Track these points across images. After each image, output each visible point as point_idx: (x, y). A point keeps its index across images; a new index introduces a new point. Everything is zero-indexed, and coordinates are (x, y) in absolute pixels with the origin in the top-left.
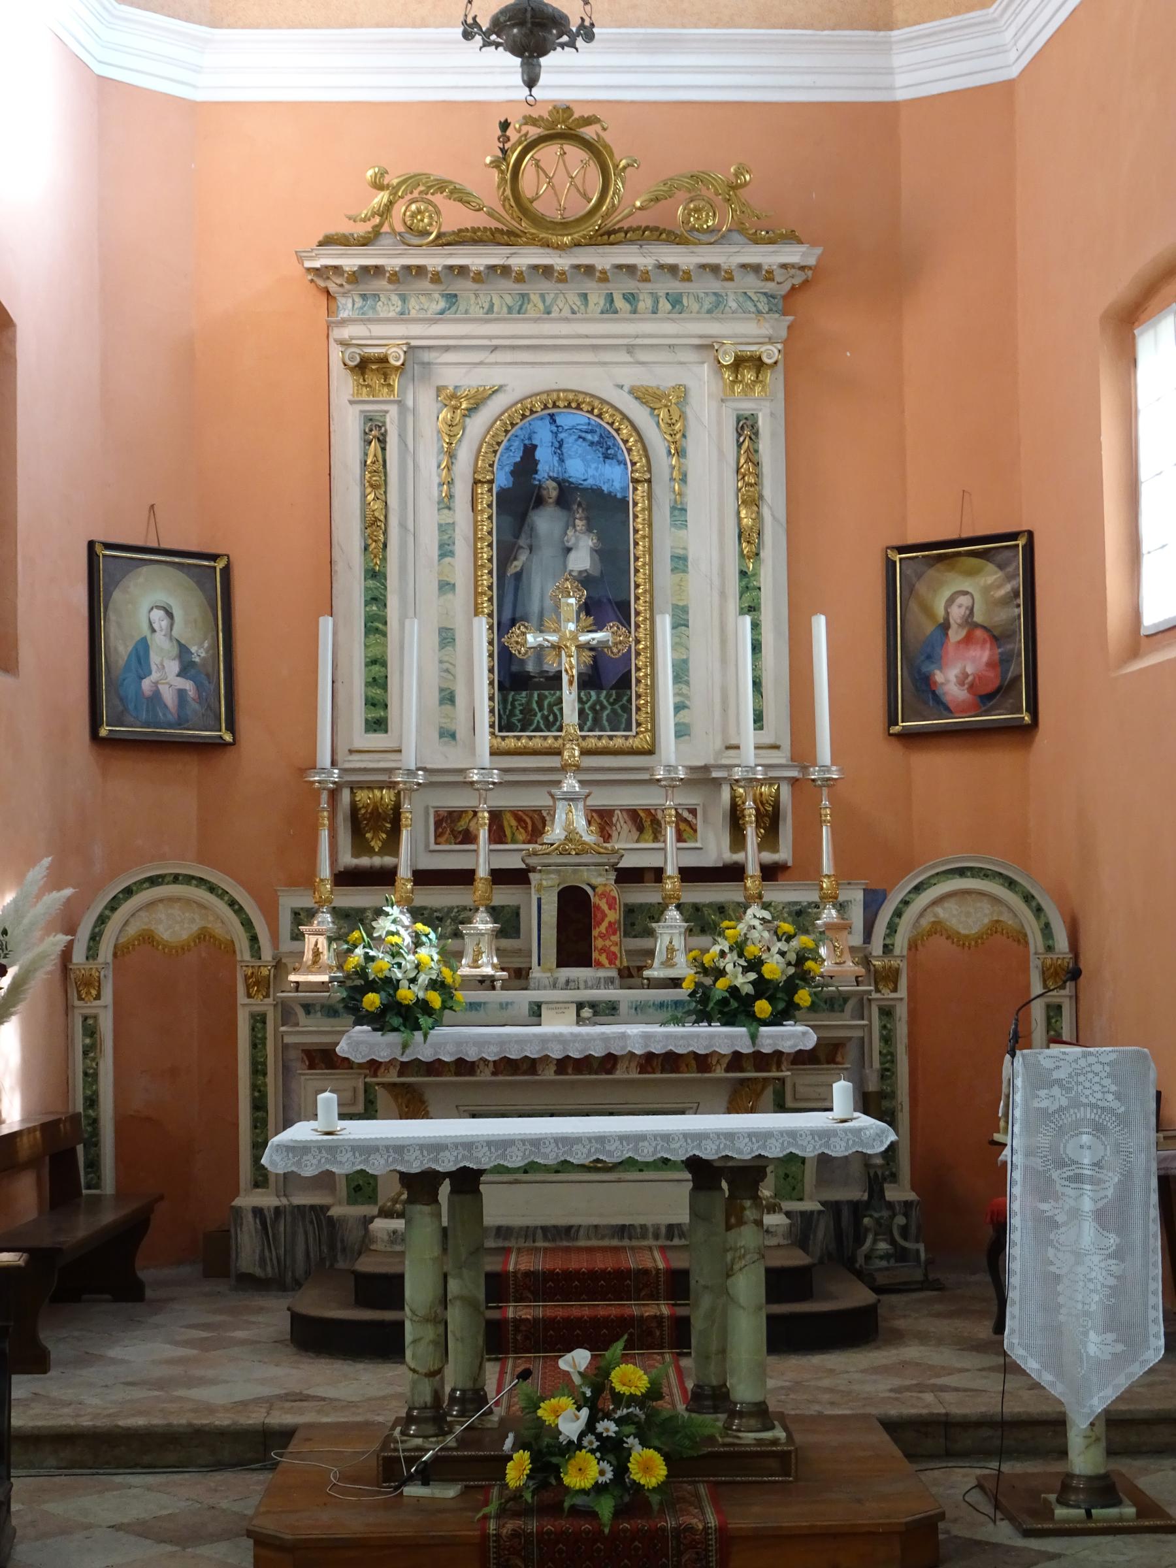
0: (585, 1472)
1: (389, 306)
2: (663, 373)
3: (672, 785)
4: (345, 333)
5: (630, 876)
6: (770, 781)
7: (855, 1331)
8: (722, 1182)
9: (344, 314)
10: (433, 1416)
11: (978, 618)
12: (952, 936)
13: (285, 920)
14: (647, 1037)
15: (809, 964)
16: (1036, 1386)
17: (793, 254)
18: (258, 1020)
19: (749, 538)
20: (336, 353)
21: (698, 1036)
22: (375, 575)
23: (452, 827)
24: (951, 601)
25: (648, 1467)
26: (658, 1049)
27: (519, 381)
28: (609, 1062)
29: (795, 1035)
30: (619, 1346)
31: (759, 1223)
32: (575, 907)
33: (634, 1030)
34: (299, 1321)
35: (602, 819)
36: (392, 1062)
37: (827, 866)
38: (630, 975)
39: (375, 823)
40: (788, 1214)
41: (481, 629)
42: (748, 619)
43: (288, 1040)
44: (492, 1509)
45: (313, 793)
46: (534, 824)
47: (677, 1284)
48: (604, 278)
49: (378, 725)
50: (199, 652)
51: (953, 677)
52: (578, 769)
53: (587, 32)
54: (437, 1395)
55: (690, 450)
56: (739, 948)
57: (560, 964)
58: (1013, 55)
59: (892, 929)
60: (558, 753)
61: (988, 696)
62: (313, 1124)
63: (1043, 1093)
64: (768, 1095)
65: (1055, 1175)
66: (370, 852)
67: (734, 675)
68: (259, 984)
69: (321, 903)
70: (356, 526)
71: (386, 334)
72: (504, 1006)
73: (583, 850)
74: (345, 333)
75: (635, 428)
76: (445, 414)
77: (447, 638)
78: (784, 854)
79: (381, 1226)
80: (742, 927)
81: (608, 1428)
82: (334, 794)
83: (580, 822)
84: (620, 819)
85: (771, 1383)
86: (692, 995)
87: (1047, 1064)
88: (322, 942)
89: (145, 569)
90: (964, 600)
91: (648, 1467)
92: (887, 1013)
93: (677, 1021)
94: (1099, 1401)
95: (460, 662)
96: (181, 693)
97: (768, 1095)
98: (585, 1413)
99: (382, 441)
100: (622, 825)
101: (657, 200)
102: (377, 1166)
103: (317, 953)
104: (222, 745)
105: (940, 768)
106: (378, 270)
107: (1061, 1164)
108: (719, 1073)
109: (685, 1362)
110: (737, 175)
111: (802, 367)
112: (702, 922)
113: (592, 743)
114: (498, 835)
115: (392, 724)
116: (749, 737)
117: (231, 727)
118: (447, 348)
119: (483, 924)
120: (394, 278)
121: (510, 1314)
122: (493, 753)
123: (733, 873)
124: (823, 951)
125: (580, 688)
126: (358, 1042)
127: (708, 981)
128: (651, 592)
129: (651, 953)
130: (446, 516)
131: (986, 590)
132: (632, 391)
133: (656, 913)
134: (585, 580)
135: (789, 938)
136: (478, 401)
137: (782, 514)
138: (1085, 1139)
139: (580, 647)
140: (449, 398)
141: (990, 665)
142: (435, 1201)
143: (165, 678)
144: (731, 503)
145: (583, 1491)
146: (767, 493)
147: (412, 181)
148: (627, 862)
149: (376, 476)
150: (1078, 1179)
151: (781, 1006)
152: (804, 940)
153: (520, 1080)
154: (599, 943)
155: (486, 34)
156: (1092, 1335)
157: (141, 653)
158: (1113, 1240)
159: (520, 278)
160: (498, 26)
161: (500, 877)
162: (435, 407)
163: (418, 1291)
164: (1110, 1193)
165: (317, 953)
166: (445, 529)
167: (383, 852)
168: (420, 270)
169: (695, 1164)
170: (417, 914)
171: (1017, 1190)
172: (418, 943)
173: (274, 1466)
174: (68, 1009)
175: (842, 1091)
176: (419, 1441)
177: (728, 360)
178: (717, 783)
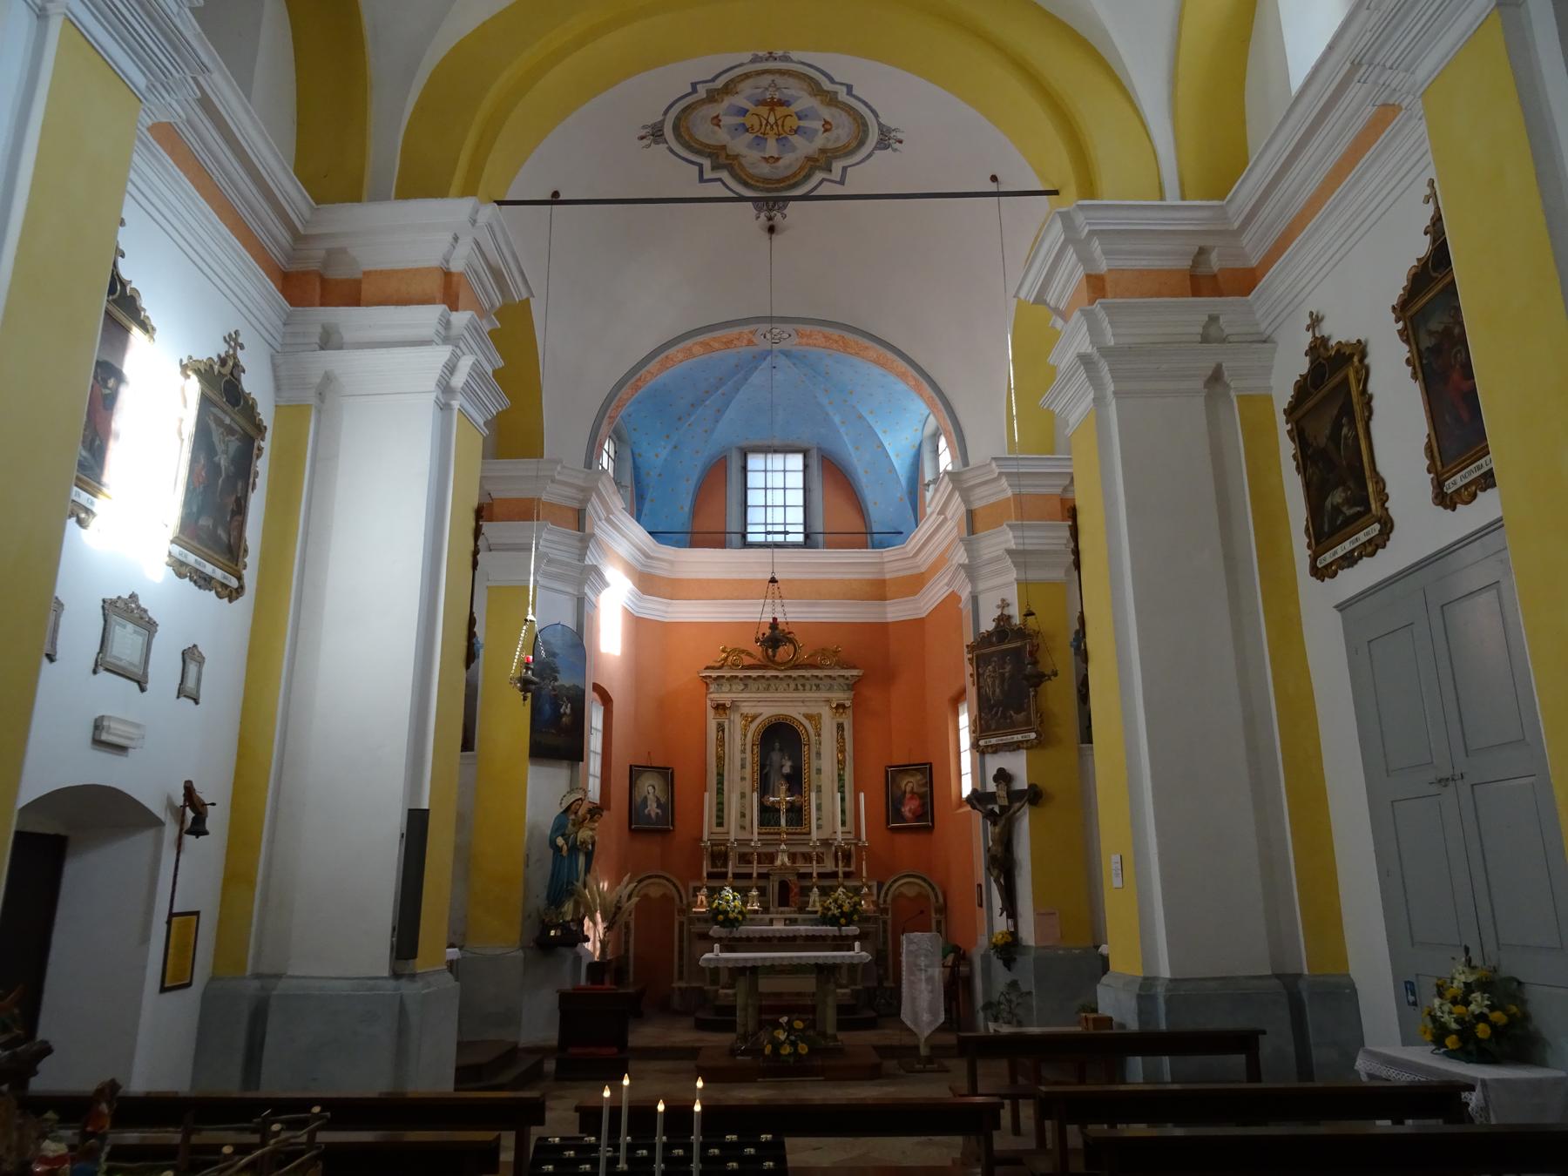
0: (786, 1050)
1: (726, 687)
2: (813, 706)
3: (814, 847)
17: (855, 672)
18: (681, 924)
19: (841, 763)
22: (720, 775)
23: (744, 859)
25: (803, 1049)
28: (794, 938)
29: (853, 930)
32: (784, 887)
35: (793, 857)
38: (802, 910)
39: (719, 857)
41: (755, 795)
46: (771, 858)
49: (720, 824)
50: (663, 800)
51: (906, 810)
56: (836, 901)
67: (835, 809)
68: (682, 911)
71: (725, 697)
77: (743, 795)
78: (852, 869)
91: (803, 1049)
92: (885, 923)
100: (799, 858)
104: (668, 831)
105: (904, 840)
112: (825, 892)
114: (759, 862)
116: (839, 829)
119: (754, 893)
123: (834, 875)
126: (715, 930)
133: (810, 889)
136: (754, 718)
143: (652, 809)
147: (734, 650)
149: (721, 742)
153: (766, 942)
161: (760, 876)
166: (743, 760)
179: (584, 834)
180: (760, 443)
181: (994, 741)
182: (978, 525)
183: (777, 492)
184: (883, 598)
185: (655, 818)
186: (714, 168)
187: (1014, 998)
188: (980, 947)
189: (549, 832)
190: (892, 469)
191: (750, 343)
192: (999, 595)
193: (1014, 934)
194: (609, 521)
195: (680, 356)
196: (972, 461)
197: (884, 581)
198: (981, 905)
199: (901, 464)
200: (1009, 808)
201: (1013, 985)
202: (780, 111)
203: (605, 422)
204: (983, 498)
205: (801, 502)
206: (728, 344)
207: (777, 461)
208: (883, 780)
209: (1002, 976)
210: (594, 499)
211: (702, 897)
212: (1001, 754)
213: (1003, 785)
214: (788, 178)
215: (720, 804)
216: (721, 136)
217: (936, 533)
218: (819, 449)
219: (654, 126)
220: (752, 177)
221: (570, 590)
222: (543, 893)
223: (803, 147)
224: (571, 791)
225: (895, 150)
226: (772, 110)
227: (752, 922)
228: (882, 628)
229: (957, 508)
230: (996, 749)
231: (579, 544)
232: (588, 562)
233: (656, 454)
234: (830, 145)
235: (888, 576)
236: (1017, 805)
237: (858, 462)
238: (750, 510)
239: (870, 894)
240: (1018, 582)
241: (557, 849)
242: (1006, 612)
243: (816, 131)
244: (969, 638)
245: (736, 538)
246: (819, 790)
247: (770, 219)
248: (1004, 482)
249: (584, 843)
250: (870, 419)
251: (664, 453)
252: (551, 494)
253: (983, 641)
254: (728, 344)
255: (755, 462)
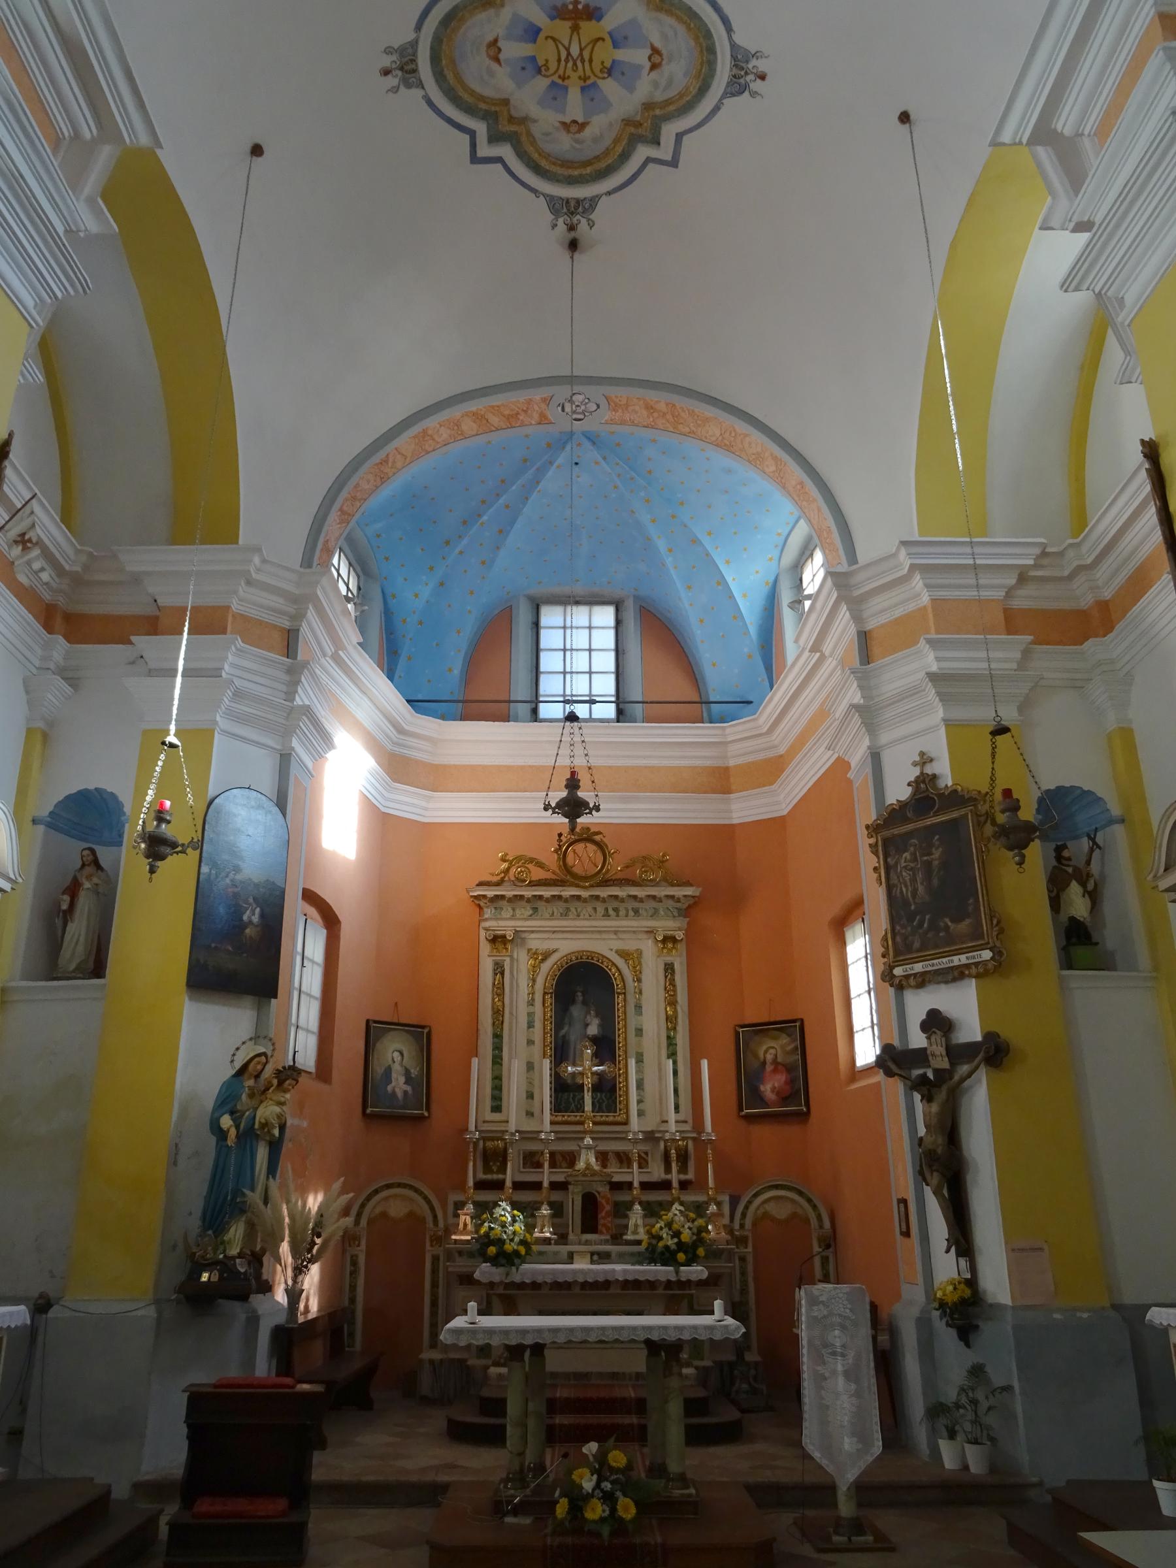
0: (595, 1511)
1: (507, 912)
3: (635, 1141)
4: (487, 924)
5: (616, 1186)
6: (683, 1139)
7: (729, 1434)
8: (662, 1351)
9: (486, 916)
10: (519, 1477)
11: (779, 1060)
12: (773, 1219)
13: (451, 1208)
14: (625, 1271)
15: (704, 1234)
16: (821, 1467)
17: (689, 891)
18: (436, 1259)
19: (671, 1020)
20: (483, 933)
21: (650, 1271)
22: (498, 1036)
23: (532, 1160)
24: (766, 1052)
26: (630, 1278)
27: (566, 947)
28: (607, 1284)
29: (697, 1271)
30: (612, 1439)
31: (680, 1374)
32: (590, 1203)
33: (618, 1267)
34: (451, 1423)
35: (603, 1157)
36: (501, 1282)
37: (711, 1183)
38: (617, 1238)
39: (495, 1157)
40: (696, 1368)
41: (547, 1063)
42: (671, 1061)
43: (450, 1269)
44: (549, 1530)
45: (466, 1143)
46: (571, 1159)
47: (640, 1406)
48: (604, 900)
49: (497, 1109)
50: (414, 1072)
51: (769, 1087)
52: (592, 1132)
53: (597, 808)
54: (522, 1465)
55: (643, 978)
56: (669, 1225)
57: (583, 1232)
58: (784, 806)
59: (744, 1215)
60: (582, 1123)
61: (786, 1098)
62: (464, 1318)
63: (815, 1308)
64: (685, 1304)
65: (823, 1351)
66: (492, 1172)
67: (663, 1087)
69: (468, 1199)
70: (490, 1013)
71: (505, 925)
72: (556, 1253)
73: (594, 1173)
74: (487, 924)
75: (618, 969)
76: (531, 962)
77: (530, 1066)
78: (690, 1176)
79: (493, 1370)
80: (670, 1214)
81: (607, 1486)
82: (476, 1144)
83: (593, 1160)
84: (611, 1156)
85: (688, 1462)
86: (647, 1249)
87: (816, 1293)
88: (468, 1219)
89: (392, 1033)
90: (773, 1051)
91: (627, 1509)
92: (743, 1259)
93: (641, 1263)
94: (851, 1475)
95: (536, 1083)
96: (405, 1092)
97: (685, 1304)
98: (595, 1477)
99: (502, 973)
100: (613, 1160)
101: (627, 867)
102: (495, 1342)
103: (465, 1225)
104: (421, 1118)
105: (763, 1133)
106: (503, 897)
107: (826, 1346)
108: (660, 1291)
109: (646, 1450)
110: (664, 856)
111: (695, 942)
112: (652, 1211)
113: (598, 1119)
114: (553, 1164)
115: (504, 1108)
116: (672, 1116)
117: (428, 1109)
118: (533, 932)
119: (545, 1211)
120: (510, 900)
121: (557, 1421)
122: (552, 1123)
123: (665, 1185)
124: (710, 1227)
125: (593, 1091)
126: (484, 1271)
127: (654, 1242)
128: (626, 1045)
129: (626, 1227)
130: (531, 1009)
131: (782, 1047)
132: (617, 952)
133: (629, 1206)
134: (595, 1040)
135: (693, 1221)
136: (546, 955)
137: (686, 1009)
138: (837, 1332)
139: (593, 1073)
140: (533, 954)
141: (786, 1083)
142: (522, 1360)
143: (399, 1085)
144: (663, 1005)
145: (594, 1521)
146: (679, 998)
147: (518, 858)
148: (616, 1178)
149: (499, 990)
150: (834, 1354)
151: (690, 1255)
152: (700, 1222)
154: (601, 1222)
155: (553, 809)
156: (847, 1440)
157: (388, 1071)
158: (853, 1386)
159: (566, 901)
160: (558, 805)
161: (554, 1186)
162: (527, 958)
163: (513, 1408)
164: (850, 1361)
165: (465, 1225)
167: (498, 1172)
168: (522, 897)
169: (649, 1343)
170: (515, 1205)
171: (805, 1359)
172: (514, 1221)
173: (439, 1505)
174: (344, 1251)
175: (718, 1305)
176: (512, 1492)
177: (660, 938)
178: (658, 1140)
179: (267, 1111)
180: (557, 590)
181: (918, 967)
182: (876, 650)
183: (580, 653)
184: (727, 791)
185: (399, 1097)
186: (494, 138)
187: (980, 1395)
188: (909, 1306)
189: (210, 1104)
190: (738, 615)
191: (543, 420)
192: (920, 742)
193: (972, 1282)
194: (336, 659)
195: (445, 433)
196: (863, 557)
197: (727, 769)
198: (907, 1234)
199: (750, 608)
200: (950, 1073)
201: (977, 1372)
202: (589, 29)
203: (333, 516)
204: (882, 612)
205: (612, 668)
206: (512, 420)
207: (580, 615)
208: (732, 1047)
209: (955, 1359)
210: (311, 614)
211: (465, 1218)
212: (931, 988)
213: (938, 1036)
214: (597, 158)
215: (497, 1079)
216: (499, 82)
217: (813, 680)
218: (637, 598)
219: (402, 51)
220: (547, 156)
221: (270, 742)
222: (197, 1206)
223: (622, 100)
224: (255, 1039)
225: (754, 94)
226: (575, 29)
227: (542, 1258)
228: (725, 834)
229: (844, 629)
230: (922, 981)
231: (286, 678)
232: (298, 701)
233: (415, 595)
234: (659, 97)
235: (732, 763)
236: (964, 1069)
237: (689, 608)
238: (542, 678)
239: (720, 1214)
240: (948, 723)
241: (221, 1134)
242: (929, 770)
243: (639, 68)
244: (867, 814)
245: (524, 709)
246: (640, 1060)
247: (572, 228)
248: (917, 582)
249: (265, 1125)
250: (706, 542)
251: (426, 592)
252: (243, 601)
253: (895, 815)
254: (512, 420)
255: (551, 616)
